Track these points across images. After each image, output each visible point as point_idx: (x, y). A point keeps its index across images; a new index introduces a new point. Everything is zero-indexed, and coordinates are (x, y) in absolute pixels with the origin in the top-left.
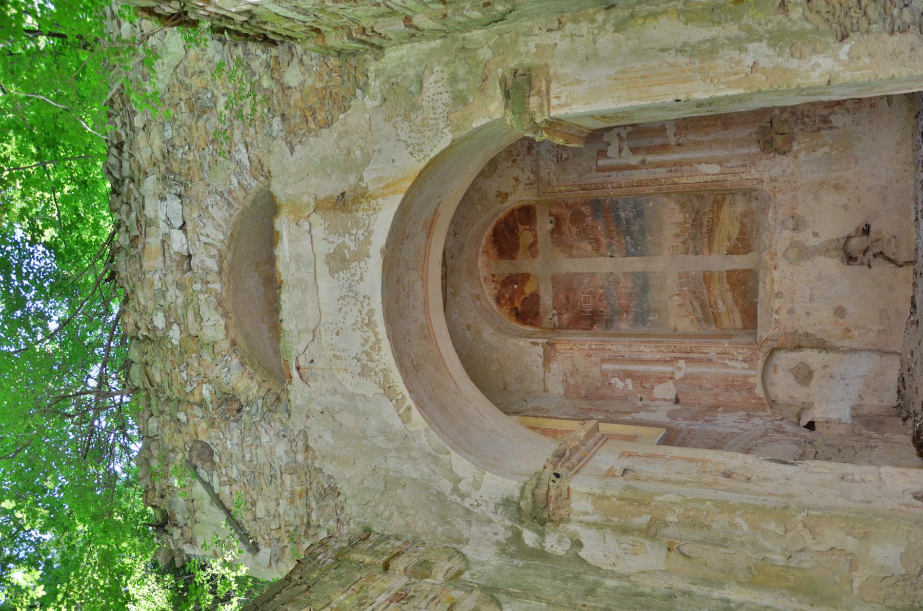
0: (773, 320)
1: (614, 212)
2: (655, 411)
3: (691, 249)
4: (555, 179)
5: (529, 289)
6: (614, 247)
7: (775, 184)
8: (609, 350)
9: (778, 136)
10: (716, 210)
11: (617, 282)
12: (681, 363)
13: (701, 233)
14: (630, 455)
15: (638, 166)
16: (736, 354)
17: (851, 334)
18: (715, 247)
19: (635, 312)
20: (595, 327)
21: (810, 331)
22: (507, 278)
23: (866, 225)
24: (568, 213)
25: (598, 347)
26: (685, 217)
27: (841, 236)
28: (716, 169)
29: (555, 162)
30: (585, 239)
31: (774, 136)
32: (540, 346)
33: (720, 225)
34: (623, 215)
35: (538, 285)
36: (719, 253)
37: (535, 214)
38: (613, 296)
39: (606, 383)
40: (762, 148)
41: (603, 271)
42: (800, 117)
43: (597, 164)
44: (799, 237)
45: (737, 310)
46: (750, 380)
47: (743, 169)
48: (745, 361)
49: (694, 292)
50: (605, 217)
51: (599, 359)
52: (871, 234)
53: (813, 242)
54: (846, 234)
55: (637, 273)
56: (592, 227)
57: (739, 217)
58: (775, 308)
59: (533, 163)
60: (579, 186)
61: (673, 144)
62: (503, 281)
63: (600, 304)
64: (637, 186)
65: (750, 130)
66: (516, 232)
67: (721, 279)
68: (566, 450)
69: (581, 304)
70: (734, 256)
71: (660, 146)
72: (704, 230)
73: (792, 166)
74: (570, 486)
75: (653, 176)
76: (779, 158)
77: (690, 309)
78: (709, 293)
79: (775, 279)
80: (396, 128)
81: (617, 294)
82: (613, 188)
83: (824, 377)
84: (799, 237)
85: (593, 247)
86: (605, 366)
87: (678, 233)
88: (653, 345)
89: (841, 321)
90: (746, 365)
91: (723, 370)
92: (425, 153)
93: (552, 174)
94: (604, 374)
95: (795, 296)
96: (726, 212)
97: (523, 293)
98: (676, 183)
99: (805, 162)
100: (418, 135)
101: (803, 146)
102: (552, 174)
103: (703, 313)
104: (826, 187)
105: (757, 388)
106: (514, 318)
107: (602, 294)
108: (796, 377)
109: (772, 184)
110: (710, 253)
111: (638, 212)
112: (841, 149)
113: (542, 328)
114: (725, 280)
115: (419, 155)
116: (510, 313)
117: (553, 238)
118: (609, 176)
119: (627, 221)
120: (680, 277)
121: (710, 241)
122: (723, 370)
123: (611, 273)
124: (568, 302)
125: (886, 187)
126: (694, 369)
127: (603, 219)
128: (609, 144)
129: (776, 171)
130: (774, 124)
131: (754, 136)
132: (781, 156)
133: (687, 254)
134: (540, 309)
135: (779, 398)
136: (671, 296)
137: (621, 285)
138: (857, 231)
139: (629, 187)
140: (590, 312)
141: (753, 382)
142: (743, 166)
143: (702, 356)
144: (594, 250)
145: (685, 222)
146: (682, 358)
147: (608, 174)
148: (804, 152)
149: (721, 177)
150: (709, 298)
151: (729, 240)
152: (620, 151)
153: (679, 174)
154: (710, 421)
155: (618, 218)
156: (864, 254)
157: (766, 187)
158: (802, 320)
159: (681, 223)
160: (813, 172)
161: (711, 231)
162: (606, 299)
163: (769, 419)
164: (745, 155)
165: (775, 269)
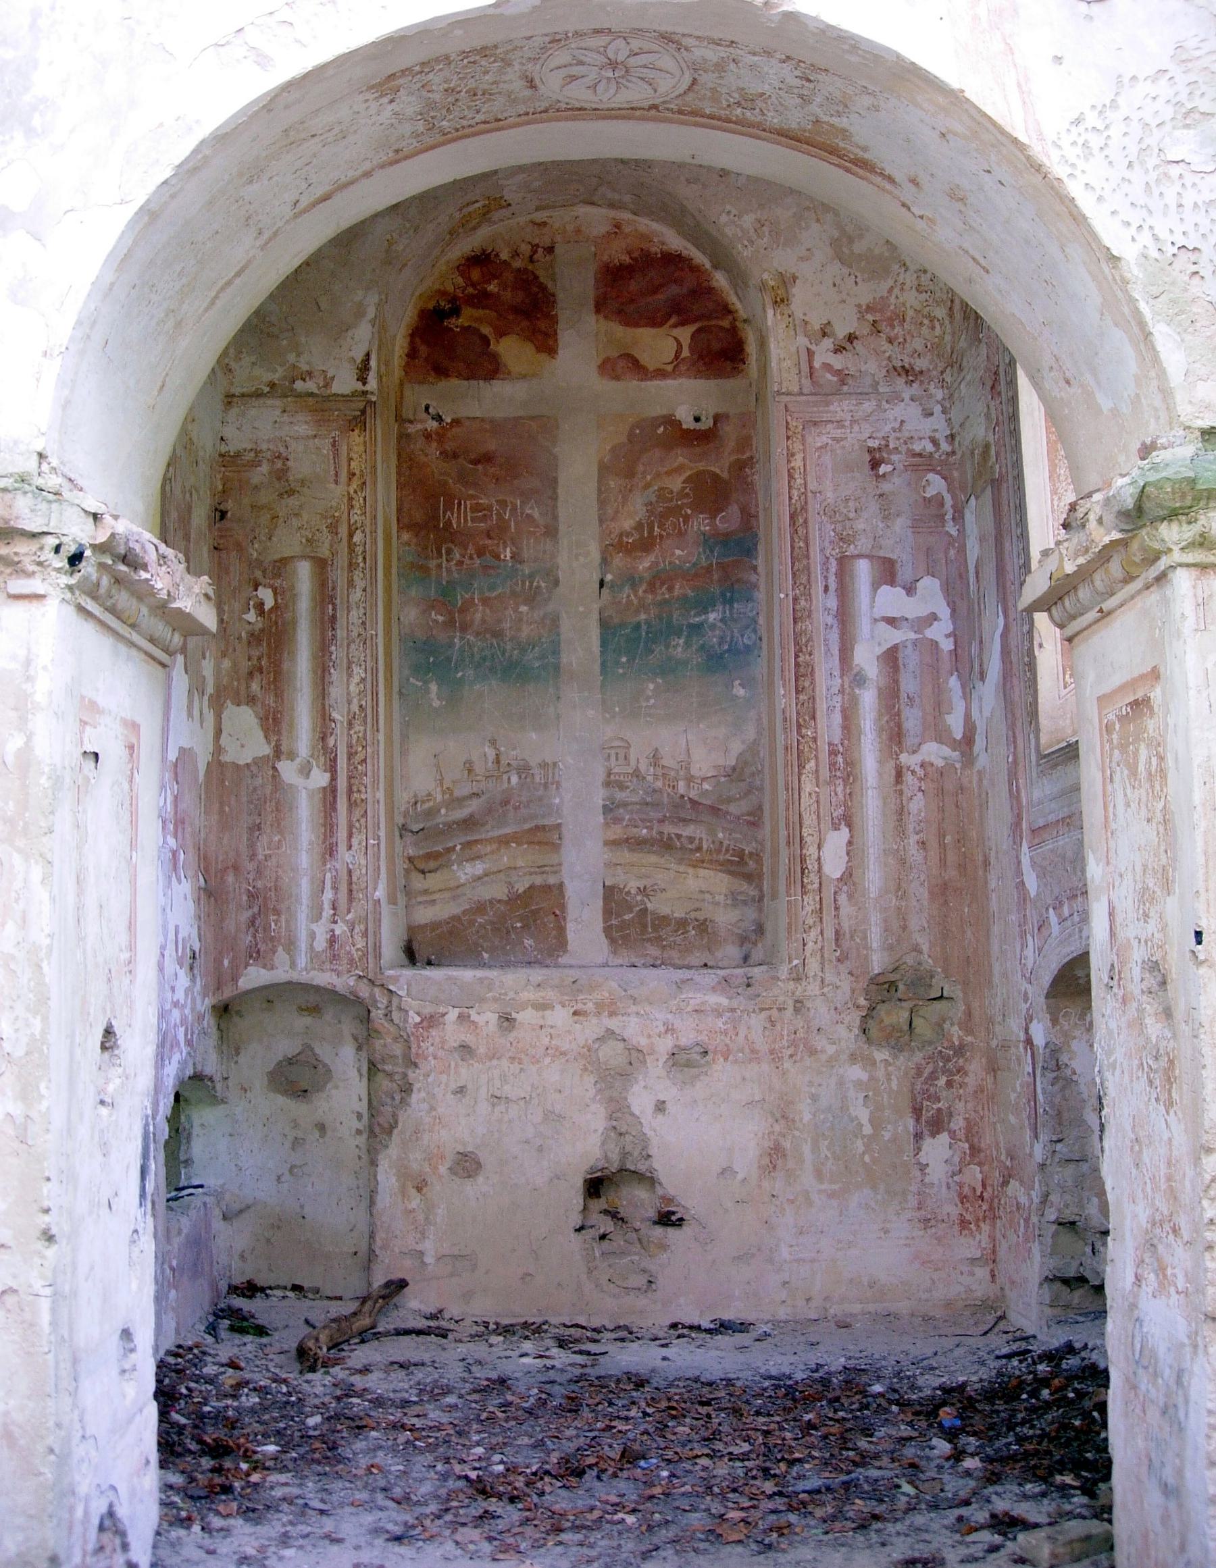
0: (442, 1010)
1: (723, 594)
2: (190, 714)
3: (620, 796)
4: (825, 439)
5: (511, 349)
6: (627, 590)
7: (790, 1011)
8: (351, 584)
9: (906, 1015)
10: (721, 858)
11: (532, 598)
12: (320, 779)
13: (661, 821)
14: (131, 748)
15: (851, 669)
16: (349, 917)
17: (413, 1192)
18: (626, 856)
19: (451, 645)
20: (406, 536)
21: (414, 1098)
22: (543, 288)
23: (681, 1219)
24: (720, 467)
25: (359, 549)
26: (704, 779)
27: (656, 1165)
28: (834, 866)
29: (871, 443)
30: (651, 512)
31: (907, 1005)
32: (359, 386)
33: (682, 868)
34: (712, 617)
35: (524, 377)
36: (608, 865)
37: (720, 374)
38: (492, 588)
39: (258, 574)
40: (881, 979)
41: (563, 560)
42: (950, 1065)
43: (859, 556)
44: (656, 1068)
45: (457, 910)
46: (281, 955)
47: (830, 934)
48: (333, 940)
49: (505, 803)
50: (709, 569)
51: (324, 552)
52: (659, 1231)
53: (640, 1101)
54: (662, 1174)
55: (556, 652)
56: (681, 534)
57: (701, 916)
58: (472, 1012)
59: (868, 380)
60: (804, 509)
61: (904, 758)
62: (536, 277)
63: (471, 550)
64: (797, 665)
65: (925, 948)
66: (673, 320)
67: (541, 869)
68: (146, 570)
69: (472, 497)
70: (600, 903)
71: (899, 725)
72: (669, 829)
73: (831, 1050)
74: (48, 601)
75: (821, 706)
76: (855, 1018)
77: (463, 790)
78: (504, 841)
79: (548, 1013)
80: (1154, 79)
81: (499, 597)
82: (795, 600)
83: (296, 1125)
84: (656, 1068)
85: (628, 534)
86: (304, 572)
87: (664, 762)
88: (367, 702)
89: (443, 1170)
90: (321, 944)
91: (305, 887)
92: (1081, 164)
93: (838, 433)
94: (282, 566)
95: (505, 1062)
96: (718, 883)
97: (501, 334)
98: (801, 766)
99: (841, 1083)
100: (1133, 150)
101: (881, 1073)
102: (838, 433)
103: (449, 826)
104: (777, 1128)
105: (263, 971)
106: (431, 306)
107: (497, 557)
108: (290, 1061)
109: (790, 1003)
110: (607, 843)
111: (721, 657)
112: (867, 1158)
113: (401, 384)
114: (538, 880)
115: (1074, 143)
116: (443, 293)
117: (657, 421)
118: (826, 589)
119: (697, 628)
120: (544, 765)
121: (638, 844)
122: (305, 887)
123: (557, 583)
124: (476, 462)
125: (771, 1261)
126: (305, 813)
127: (704, 563)
128: (910, 590)
129: (821, 1012)
130: (938, 1005)
131: (910, 960)
132: (858, 1022)
133: (607, 784)
134: (455, 382)
135: (236, 1019)
136: (493, 742)
137: (523, 609)
138: (669, 1200)
139: (797, 643)
140: (449, 523)
141: (277, 962)
142: (837, 933)
143: (342, 834)
144: (621, 535)
145: (690, 779)
146: (333, 778)
147: (833, 585)
148: (864, 1076)
149: (812, 880)
150: (489, 841)
151: (643, 891)
152: (891, 621)
153: (825, 773)
154: (175, 868)
155: (704, 606)
156: (606, 1212)
157: (783, 991)
158: (444, 1078)
159: (688, 769)
160: (814, 1098)
161: (666, 845)
162: (486, 568)
163: (187, 1011)
164: (865, 938)
165: (575, 1013)
